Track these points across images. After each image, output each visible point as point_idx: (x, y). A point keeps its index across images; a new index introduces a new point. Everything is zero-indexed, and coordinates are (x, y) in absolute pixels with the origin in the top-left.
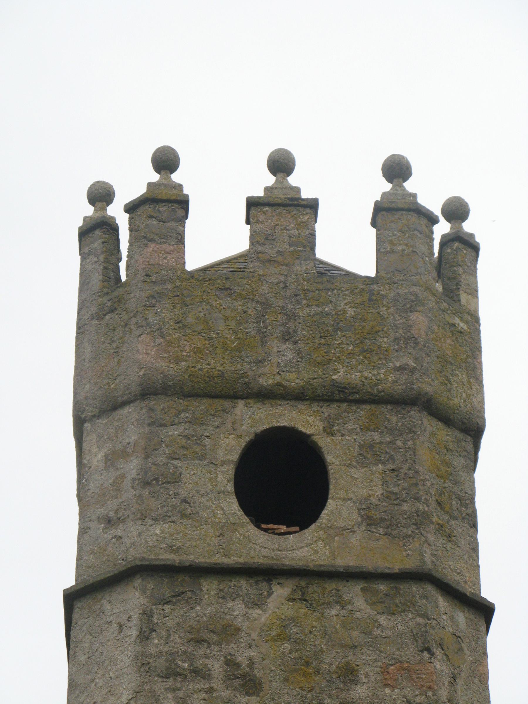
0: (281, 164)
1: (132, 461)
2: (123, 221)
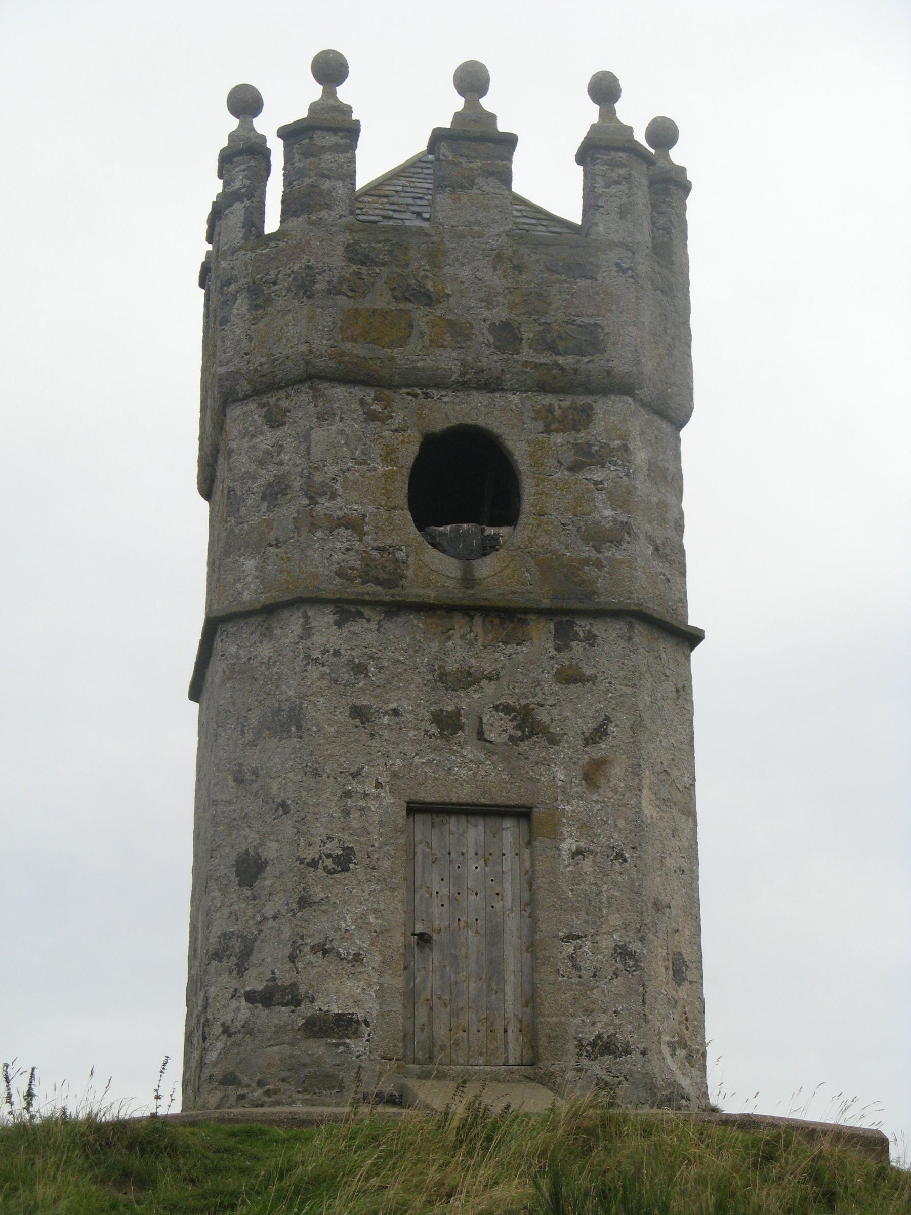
0: (472, 81)
2: (277, 148)
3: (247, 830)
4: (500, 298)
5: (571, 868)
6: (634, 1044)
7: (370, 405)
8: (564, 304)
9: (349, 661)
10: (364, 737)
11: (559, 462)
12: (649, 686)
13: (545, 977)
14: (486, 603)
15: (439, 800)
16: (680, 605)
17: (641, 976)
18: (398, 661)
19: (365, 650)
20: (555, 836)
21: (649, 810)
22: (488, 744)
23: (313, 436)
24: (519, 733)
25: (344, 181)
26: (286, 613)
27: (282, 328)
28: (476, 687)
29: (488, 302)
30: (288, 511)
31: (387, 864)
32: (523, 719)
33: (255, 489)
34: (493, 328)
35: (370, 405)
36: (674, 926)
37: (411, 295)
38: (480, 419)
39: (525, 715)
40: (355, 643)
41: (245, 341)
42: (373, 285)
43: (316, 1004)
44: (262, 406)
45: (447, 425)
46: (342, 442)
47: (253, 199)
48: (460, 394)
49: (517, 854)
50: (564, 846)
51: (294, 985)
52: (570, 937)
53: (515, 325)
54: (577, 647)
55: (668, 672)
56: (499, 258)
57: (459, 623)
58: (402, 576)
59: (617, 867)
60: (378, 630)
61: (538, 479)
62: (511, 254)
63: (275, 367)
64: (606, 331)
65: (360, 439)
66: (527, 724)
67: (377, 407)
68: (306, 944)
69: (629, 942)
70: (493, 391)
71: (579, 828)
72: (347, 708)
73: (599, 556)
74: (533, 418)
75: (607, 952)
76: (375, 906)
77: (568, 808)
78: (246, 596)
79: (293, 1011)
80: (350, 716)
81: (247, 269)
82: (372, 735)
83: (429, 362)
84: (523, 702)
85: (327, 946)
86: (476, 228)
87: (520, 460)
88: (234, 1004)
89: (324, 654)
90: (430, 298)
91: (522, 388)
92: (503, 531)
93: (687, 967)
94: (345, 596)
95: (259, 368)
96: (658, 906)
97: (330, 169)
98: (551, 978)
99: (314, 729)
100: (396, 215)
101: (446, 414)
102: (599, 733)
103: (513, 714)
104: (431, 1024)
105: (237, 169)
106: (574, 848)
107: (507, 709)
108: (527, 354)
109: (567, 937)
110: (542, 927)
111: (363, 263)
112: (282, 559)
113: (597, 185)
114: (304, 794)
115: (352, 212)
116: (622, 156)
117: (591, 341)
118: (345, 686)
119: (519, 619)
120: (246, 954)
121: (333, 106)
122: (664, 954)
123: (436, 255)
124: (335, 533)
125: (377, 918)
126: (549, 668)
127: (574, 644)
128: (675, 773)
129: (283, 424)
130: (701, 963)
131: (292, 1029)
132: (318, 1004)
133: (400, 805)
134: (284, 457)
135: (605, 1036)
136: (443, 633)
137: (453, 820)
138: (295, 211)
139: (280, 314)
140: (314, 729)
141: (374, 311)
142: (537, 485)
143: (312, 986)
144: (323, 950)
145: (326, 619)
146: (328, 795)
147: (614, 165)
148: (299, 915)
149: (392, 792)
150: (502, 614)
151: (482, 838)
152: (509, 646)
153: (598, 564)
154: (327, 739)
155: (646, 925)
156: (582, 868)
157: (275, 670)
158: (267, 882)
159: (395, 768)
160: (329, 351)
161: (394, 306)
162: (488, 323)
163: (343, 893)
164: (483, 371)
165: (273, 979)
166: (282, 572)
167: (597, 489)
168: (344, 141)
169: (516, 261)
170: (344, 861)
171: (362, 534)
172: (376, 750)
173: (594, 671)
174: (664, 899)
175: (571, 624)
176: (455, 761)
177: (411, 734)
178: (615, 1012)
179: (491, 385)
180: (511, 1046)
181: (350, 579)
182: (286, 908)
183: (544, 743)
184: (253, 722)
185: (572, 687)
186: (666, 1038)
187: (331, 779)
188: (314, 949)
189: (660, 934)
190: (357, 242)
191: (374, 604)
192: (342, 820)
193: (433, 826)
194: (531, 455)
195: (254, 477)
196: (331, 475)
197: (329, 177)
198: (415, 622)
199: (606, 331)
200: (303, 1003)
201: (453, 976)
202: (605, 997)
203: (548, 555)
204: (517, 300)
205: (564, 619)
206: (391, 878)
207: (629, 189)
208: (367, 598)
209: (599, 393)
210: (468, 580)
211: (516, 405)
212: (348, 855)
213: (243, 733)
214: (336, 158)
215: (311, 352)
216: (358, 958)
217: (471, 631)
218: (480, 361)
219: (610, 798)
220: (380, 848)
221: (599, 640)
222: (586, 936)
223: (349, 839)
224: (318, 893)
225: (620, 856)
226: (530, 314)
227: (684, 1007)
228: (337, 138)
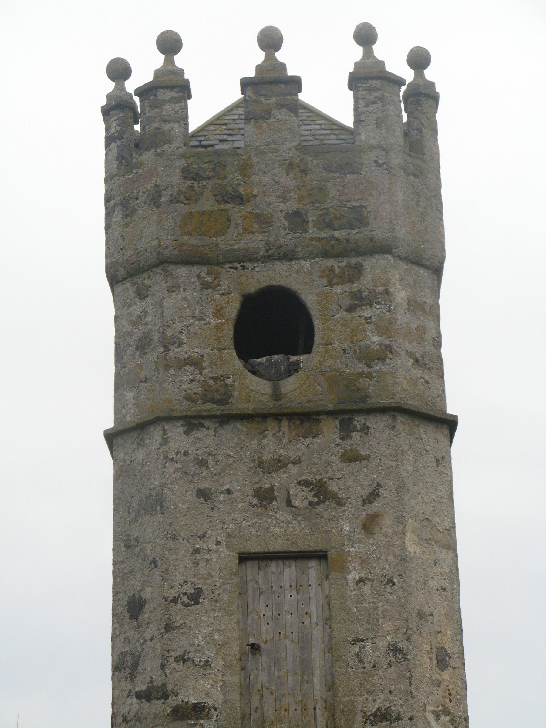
0: (270, 40)
3: (133, 580)
4: (292, 194)
5: (355, 592)
6: (404, 713)
7: (204, 278)
8: (338, 194)
9: (195, 458)
10: (207, 510)
11: (339, 306)
12: (411, 459)
13: (339, 670)
14: (289, 410)
15: (261, 550)
16: (439, 399)
17: (408, 665)
18: (229, 455)
19: (206, 450)
20: (344, 570)
21: (412, 547)
22: (294, 509)
23: (165, 304)
24: (316, 500)
25: (179, 123)
26: (152, 428)
27: (142, 230)
28: (284, 470)
29: (284, 198)
30: (152, 357)
31: (225, 597)
32: (318, 490)
33: (132, 343)
34: (287, 216)
35: (204, 278)
36: (437, 628)
37: (229, 198)
38: (282, 281)
39: (320, 487)
40: (199, 445)
41: (120, 240)
42: (202, 194)
43: (179, 697)
44: (134, 284)
45: (259, 287)
46: (186, 306)
47: (123, 140)
48: (267, 264)
49: (319, 585)
50: (350, 577)
51: (164, 685)
52: (356, 641)
53: (304, 212)
54: (356, 436)
55: (428, 448)
56: (290, 165)
57: (271, 426)
58: (231, 396)
59: (388, 589)
60: (215, 435)
61: (325, 319)
62: (299, 162)
63: (139, 257)
64: (369, 210)
65: (198, 303)
66: (321, 492)
67: (209, 279)
68: (171, 656)
69: (399, 642)
70: (291, 260)
71: (360, 563)
72: (194, 491)
73: (370, 370)
74: (319, 277)
75: (382, 649)
76: (218, 627)
77: (352, 550)
78: (128, 418)
79: (164, 703)
80: (197, 496)
81: (120, 190)
82: (213, 508)
83: (242, 244)
84: (318, 478)
85: (186, 657)
86: (273, 146)
87: (311, 307)
88: (129, 701)
89: (177, 455)
90: (242, 199)
91: (311, 256)
92: (303, 358)
93: (450, 657)
94: (189, 413)
95: (129, 258)
96: (421, 615)
97: (169, 115)
98: (343, 670)
99: (172, 507)
100: (230, 138)
101: (258, 279)
102: (374, 495)
103: (311, 487)
104: (262, 707)
105: (112, 119)
106: (357, 578)
107: (307, 483)
108: (312, 232)
109: (354, 641)
110: (336, 634)
111: (194, 179)
112: (149, 391)
113: (359, 106)
114: (166, 552)
115: (185, 144)
116: (377, 83)
117: (359, 218)
118: (192, 476)
119: (314, 419)
120: (135, 666)
121: (170, 71)
122: (428, 649)
123: (245, 169)
124: (183, 370)
125: (219, 635)
126: (336, 452)
127: (353, 434)
128: (435, 519)
129: (147, 296)
130: (463, 654)
131: (164, 715)
132: (180, 698)
133: (233, 556)
134: (149, 319)
135: (383, 709)
136: (260, 433)
137: (274, 563)
138: (147, 147)
139: (141, 220)
140: (172, 507)
141: (203, 213)
142: (324, 324)
143: (176, 685)
144: (183, 659)
145: (178, 431)
146: (183, 552)
147: (371, 90)
148: (166, 636)
149: (228, 547)
150: (302, 417)
151: (294, 575)
152: (307, 439)
153: (369, 376)
154: (181, 514)
155: (411, 629)
156: (363, 591)
157: (147, 468)
158: (146, 615)
159: (229, 530)
160: (173, 243)
161: (217, 207)
162: (284, 212)
163: (196, 619)
164: (281, 247)
165: (152, 682)
166: (149, 399)
167: (368, 323)
168: (179, 94)
169: (302, 167)
170: (195, 597)
171: (201, 369)
172: (215, 518)
173: (368, 452)
174: (427, 609)
175: (351, 420)
176: (272, 522)
177: (240, 506)
178: (390, 691)
179: (289, 256)
180: (319, 719)
181: (194, 401)
182: (158, 632)
183: (334, 505)
184: (135, 505)
185: (353, 464)
186: (430, 708)
187: (185, 541)
188: (177, 659)
189: (424, 635)
190: (189, 165)
191: (211, 417)
192: (194, 569)
193: (259, 569)
194: (319, 303)
195: (131, 335)
196: (178, 330)
197: (169, 121)
198: (240, 427)
199: (369, 210)
200: (170, 697)
201: (276, 673)
202: (383, 681)
203: (334, 372)
204: (304, 194)
205: (346, 417)
206: (229, 607)
207: (383, 106)
208: (204, 413)
209: (366, 254)
210: (277, 395)
211: (307, 268)
212: (198, 593)
213: (129, 513)
214: (173, 107)
215: (160, 245)
216: (207, 664)
217: (280, 431)
218: (279, 240)
219: (382, 541)
220: (220, 586)
221: (371, 430)
222: (367, 639)
223: (199, 582)
224: (178, 620)
225: (391, 581)
226: (314, 203)
227: (448, 686)
228: (173, 92)
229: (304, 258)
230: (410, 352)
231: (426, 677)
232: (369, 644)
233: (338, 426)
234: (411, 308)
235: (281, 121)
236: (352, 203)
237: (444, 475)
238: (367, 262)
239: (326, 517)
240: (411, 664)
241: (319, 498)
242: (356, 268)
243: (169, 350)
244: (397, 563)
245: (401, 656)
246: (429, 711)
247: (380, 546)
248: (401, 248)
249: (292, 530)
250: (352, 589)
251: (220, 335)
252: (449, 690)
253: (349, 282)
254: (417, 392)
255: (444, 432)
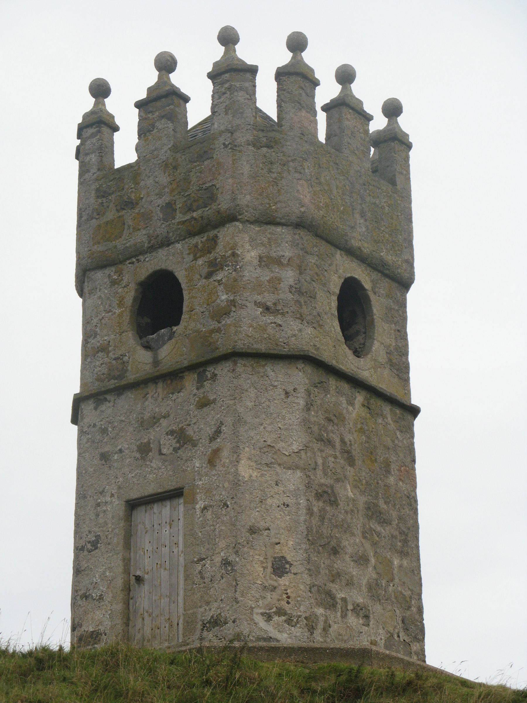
1: (287, 271)
4: (166, 189)
7: (113, 276)
18: (122, 421)
19: (107, 419)
20: (194, 501)
21: (246, 470)
24: (178, 445)
28: (158, 424)
29: (160, 195)
37: (124, 206)
40: (103, 417)
46: (100, 303)
48: (154, 254)
50: (198, 506)
54: (207, 384)
57: (151, 389)
58: (127, 370)
59: (224, 512)
65: (108, 298)
66: (182, 438)
70: (168, 245)
73: (219, 325)
76: (109, 565)
77: (200, 483)
83: (132, 242)
84: (180, 426)
90: (132, 203)
91: (182, 238)
93: (291, 565)
103: (175, 435)
106: (202, 506)
111: (103, 197)
118: (98, 443)
122: (262, 559)
125: (110, 572)
135: (215, 616)
142: (189, 294)
145: (90, 408)
155: (239, 543)
164: (158, 236)
168: (96, 129)
178: (221, 600)
179: (166, 243)
185: (205, 409)
194: (187, 277)
199: (217, 187)
205: (201, 369)
211: (180, 249)
216: (101, 598)
217: (156, 392)
219: (221, 471)
220: (112, 531)
225: (226, 505)
227: (286, 590)
229: (177, 241)
230: (259, 302)
231: (256, 583)
232: (209, 562)
233: (196, 379)
234: (263, 264)
235: (161, 130)
236: (206, 185)
237: (294, 405)
238: (221, 232)
239: (184, 458)
240: (237, 574)
241: (180, 443)
242: (213, 239)
243: (88, 342)
244: (231, 488)
245: (229, 568)
246: (257, 614)
247: (220, 476)
248: (246, 214)
249: (161, 474)
250: (199, 516)
251: (121, 321)
252: (287, 594)
253: (208, 253)
254: (265, 336)
255: (299, 367)
